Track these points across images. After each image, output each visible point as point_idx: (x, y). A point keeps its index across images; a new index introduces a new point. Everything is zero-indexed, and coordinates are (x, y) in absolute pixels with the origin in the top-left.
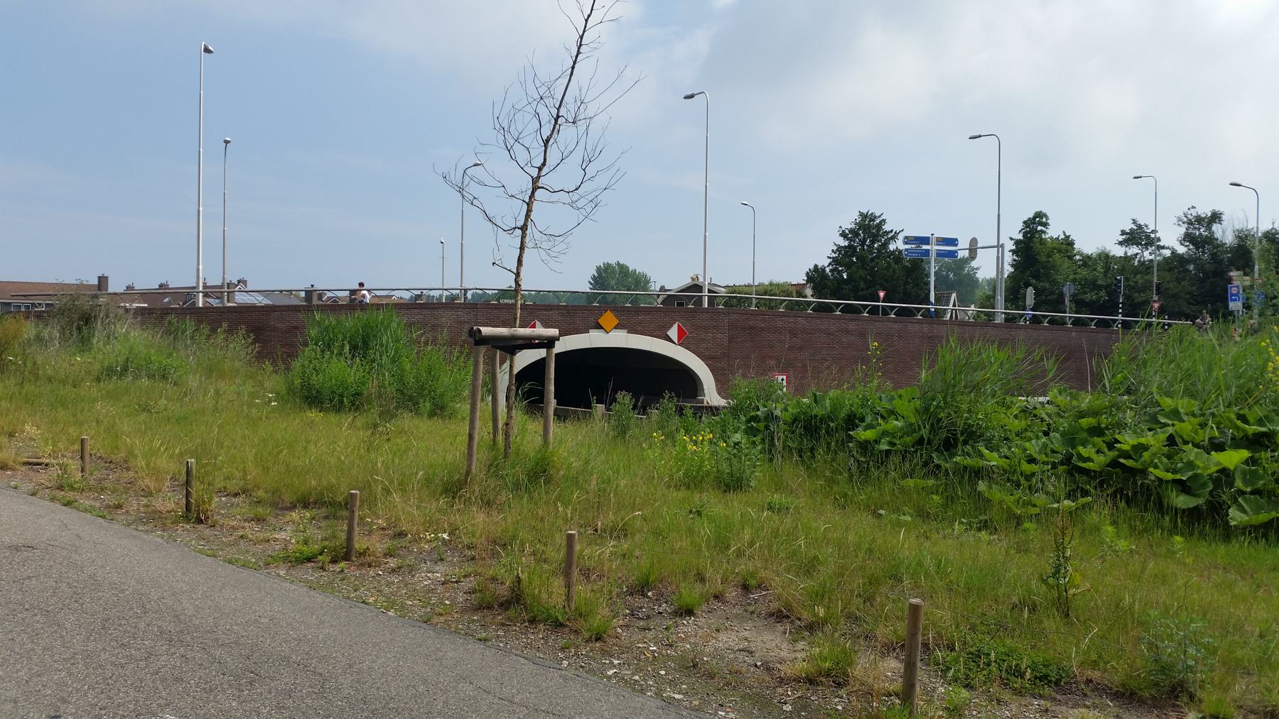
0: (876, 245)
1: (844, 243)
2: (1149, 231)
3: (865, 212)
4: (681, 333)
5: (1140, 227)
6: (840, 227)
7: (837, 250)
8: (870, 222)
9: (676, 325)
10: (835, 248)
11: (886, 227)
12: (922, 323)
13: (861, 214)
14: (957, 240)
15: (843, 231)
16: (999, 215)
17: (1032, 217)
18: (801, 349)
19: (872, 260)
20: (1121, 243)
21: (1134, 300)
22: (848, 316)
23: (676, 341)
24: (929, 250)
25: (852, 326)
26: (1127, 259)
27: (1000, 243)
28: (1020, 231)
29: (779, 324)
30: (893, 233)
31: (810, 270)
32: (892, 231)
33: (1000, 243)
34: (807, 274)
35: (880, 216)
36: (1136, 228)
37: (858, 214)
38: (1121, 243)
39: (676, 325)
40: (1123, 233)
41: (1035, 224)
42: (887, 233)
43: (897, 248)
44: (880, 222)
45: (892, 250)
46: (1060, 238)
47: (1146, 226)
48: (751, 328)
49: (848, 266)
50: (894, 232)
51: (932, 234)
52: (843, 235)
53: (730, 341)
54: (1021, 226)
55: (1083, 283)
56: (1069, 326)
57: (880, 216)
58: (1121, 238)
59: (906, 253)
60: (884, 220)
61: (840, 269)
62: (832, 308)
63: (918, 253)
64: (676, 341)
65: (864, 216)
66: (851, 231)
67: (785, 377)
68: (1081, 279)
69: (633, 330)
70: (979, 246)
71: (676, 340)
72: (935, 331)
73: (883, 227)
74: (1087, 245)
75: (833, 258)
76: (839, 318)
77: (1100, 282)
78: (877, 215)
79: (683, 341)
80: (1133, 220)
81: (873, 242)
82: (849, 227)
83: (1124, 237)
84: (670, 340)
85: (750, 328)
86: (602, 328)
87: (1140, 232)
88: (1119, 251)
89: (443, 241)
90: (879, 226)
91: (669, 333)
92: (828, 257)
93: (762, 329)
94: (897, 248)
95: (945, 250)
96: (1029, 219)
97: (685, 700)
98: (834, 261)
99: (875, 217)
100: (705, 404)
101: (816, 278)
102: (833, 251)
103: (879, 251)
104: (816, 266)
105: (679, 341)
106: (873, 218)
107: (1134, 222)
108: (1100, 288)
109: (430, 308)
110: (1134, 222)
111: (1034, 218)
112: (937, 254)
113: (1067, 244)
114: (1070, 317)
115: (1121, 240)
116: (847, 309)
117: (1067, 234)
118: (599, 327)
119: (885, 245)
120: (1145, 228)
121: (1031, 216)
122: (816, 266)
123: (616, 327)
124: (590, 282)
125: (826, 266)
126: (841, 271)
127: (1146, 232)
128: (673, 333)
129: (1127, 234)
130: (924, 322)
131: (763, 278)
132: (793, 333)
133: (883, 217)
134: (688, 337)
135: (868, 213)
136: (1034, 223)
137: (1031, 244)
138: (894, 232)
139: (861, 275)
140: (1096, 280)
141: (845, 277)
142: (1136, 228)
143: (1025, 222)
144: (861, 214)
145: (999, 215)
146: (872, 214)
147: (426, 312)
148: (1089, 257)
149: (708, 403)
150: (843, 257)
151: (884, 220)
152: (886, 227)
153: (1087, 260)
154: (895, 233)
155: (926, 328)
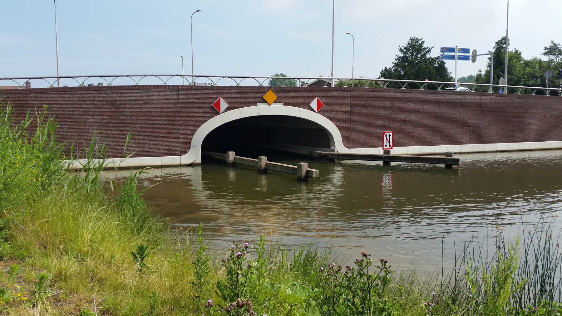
0: (419, 56)
1: (402, 55)
2: (561, 47)
3: (413, 37)
4: (319, 105)
5: (555, 45)
6: (399, 46)
7: (398, 59)
8: (415, 43)
9: (316, 99)
10: (397, 58)
11: (425, 46)
12: (475, 95)
13: (411, 39)
14: (469, 49)
15: (401, 49)
16: (507, 30)
17: (500, 40)
18: (398, 114)
19: (417, 64)
20: (544, 54)
21: (555, 84)
22: (429, 91)
23: (316, 111)
24: (454, 55)
25: (431, 98)
26: (551, 61)
27: (488, 53)
28: (494, 48)
29: (384, 97)
30: (428, 49)
31: (383, 70)
32: (428, 47)
33: (488, 53)
34: (381, 72)
35: (421, 40)
36: (553, 46)
37: (409, 38)
38: (544, 54)
39: (316, 99)
40: (546, 48)
41: (501, 45)
42: (425, 49)
43: (430, 57)
44: (422, 43)
45: (428, 58)
46: (513, 52)
47: (559, 44)
48: (366, 100)
49: (403, 68)
50: (429, 48)
51: (456, 46)
52: (401, 50)
53: (352, 109)
54: (494, 45)
55: (528, 75)
56: (548, 95)
57: (421, 40)
58: (544, 51)
59: (442, 57)
60: (423, 42)
61: (399, 69)
62: (418, 86)
63: (449, 57)
64: (316, 111)
65: (412, 40)
66: (405, 48)
67: (391, 134)
68: (527, 73)
69: (286, 103)
70: (477, 54)
71: (315, 109)
72: (483, 100)
73: (423, 46)
74: (527, 56)
75: (396, 63)
76: (422, 92)
77: (537, 75)
78: (420, 39)
79: (321, 109)
80: (552, 41)
81: (417, 54)
82: (405, 46)
83: (546, 51)
84: (311, 109)
85: (365, 100)
86: (266, 102)
87: (555, 48)
88: (545, 59)
89: (182, 56)
90: (421, 45)
91: (311, 105)
92: (393, 63)
93: (373, 101)
94: (430, 57)
95: (463, 56)
96: (499, 41)
97: (314, 247)
98: (395, 65)
99: (419, 40)
100: (336, 152)
101: (386, 73)
102: (395, 59)
103: (421, 58)
104: (386, 68)
105: (317, 110)
106: (417, 40)
107: (552, 42)
108: (537, 78)
109: (144, 89)
110: (552, 42)
111: (502, 40)
112: (459, 57)
113: (517, 55)
114: (549, 90)
115: (544, 52)
116: (429, 86)
117: (517, 49)
118: (264, 101)
119: (425, 55)
120: (558, 45)
121: (500, 39)
122: (386, 68)
123: (275, 101)
124: (269, 83)
125: (392, 67)
126: (400, 70)
127: (559, 48)
128: (314, 105)
129: (548, 49)
130: (476, 94)
131: (357, 76)
132: (393, 103)
133: (423, 40)
134: (323, 108)
135: (415, 38)
136: (502, 43)
137: (501, 54)
138: (429, 48)
139: (412, 72)
140: (535, 73)
141: (402, 74)
142: (553, 46)
143: (497, 43)
144: (411, 39)
145: (507, 30)
146: (417, 39)
147: (141, 92)
148: (529, 62)
149: (337, 152)
150: (402, 62)
151: (423, 42)
152: (425, 46)
153: (527, 64)
154: (429, 49)
155: (477, 98)
